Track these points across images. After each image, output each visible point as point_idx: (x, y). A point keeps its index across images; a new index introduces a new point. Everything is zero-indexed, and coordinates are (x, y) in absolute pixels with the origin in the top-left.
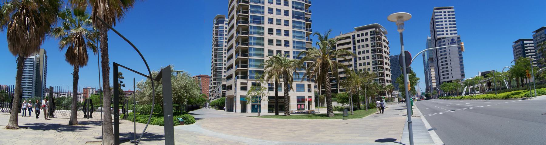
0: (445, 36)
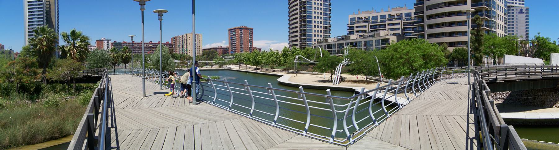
0: (514, 5)
